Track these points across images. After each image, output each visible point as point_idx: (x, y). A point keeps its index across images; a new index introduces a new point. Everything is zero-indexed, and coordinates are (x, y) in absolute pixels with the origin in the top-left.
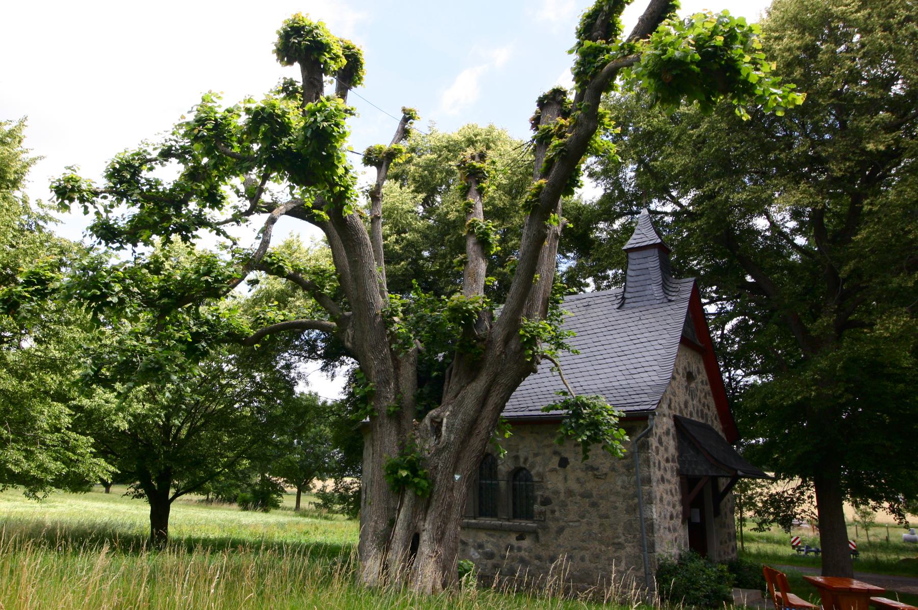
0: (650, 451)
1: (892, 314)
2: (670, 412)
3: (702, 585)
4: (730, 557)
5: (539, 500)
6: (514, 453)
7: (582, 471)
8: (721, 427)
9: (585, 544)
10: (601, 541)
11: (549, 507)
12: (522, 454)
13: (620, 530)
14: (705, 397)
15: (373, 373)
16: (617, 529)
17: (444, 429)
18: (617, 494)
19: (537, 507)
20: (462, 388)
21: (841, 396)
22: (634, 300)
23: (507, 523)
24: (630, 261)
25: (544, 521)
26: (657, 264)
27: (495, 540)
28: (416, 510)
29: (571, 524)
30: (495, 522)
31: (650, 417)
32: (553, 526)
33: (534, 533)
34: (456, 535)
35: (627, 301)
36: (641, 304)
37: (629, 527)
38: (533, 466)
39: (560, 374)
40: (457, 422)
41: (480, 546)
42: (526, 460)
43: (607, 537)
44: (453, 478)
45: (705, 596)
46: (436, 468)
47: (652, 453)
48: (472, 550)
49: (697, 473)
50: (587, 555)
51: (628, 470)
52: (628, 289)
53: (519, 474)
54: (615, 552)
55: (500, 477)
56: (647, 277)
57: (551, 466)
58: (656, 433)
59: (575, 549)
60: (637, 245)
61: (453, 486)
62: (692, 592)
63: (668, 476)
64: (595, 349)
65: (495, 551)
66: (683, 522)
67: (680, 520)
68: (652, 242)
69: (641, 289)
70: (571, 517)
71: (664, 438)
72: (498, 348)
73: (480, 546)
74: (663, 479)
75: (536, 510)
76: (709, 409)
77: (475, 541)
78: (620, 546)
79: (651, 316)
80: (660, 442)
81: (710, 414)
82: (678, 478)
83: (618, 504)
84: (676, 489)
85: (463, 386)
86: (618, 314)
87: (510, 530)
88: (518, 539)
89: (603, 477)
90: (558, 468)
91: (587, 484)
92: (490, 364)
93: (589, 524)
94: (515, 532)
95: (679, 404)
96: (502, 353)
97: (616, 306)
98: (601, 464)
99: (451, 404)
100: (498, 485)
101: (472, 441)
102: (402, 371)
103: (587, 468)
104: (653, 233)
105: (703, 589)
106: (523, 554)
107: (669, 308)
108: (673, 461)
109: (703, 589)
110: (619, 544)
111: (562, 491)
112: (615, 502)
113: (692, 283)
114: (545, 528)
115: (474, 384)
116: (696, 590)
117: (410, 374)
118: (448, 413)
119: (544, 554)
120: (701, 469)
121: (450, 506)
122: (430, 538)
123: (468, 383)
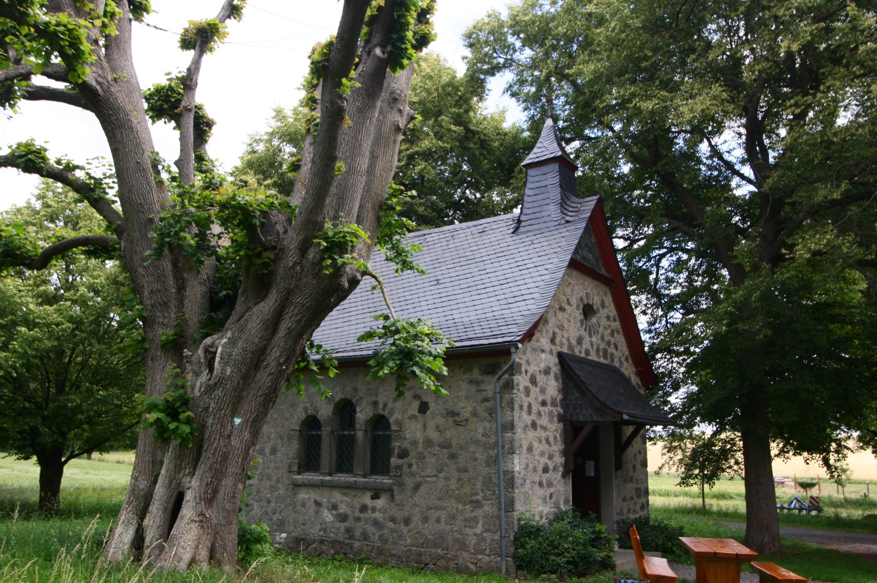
0: (515, 391)
1: (817, 232)
2: (553, 348)
3: (566, 549)
4: (637, 516)
5: (396, 452)
6: (374, 399)
7: (442, 417)
8: (634, 369)
9: (440, 503)
10: (458, 499)
11: (406, 460)
12: (381, 400)
13: (479, 486)
14: (612, 334)
15: (146, 293)
16: (475, 485)
17: (217, 359)
18: (478, 442)
19: (394, 461)
20: (249, 309)
21: (759, 331)
22: (530, 222)
23: (362, 479)
24: (529, 178)
25: (400, 476)
26: (557, 180)
27: (349, 500)
28: (181, 462)
29: (428, 479)
30: (352, 479)
31: (513, 350)
32: (409, 482)
33: (389, 490)
34: (234, 493)
35: (523, 224)
36: (537, 227)
37: (488, 482)
38: (392, 413)
39: (383, 292)
40: (236, 351)
41: (334, 507)
42: (385, 405)
43: (465, 493)
44: (232, 422)
45: (568, 562)
46: (206, 409)
47: (519, 396)
48: (326, 511)
49: (581, 418)
50: (443, 516)
51: (490, 414)
52: (525, 211)
53: (379, 422)
54: (472, 511)
55: (357, 426)
56: (546, 196)
57: (410, 412)
58: (526, 372)
59: (431, 508)
60: (537, 160)
61: (231, 433)
62: (553, 557)
63: (544, 421)
64: (479, 278)
65: (349, 513)
66: (564, 476)
67: (560, 474)
68: (552, 156)
69: (538, 209)
70: (428, 471)
71: (540, 378)
72: (291, 257)
73: (334, 507)
74: (534, 425)
75: (392, 464)
76: (616, 348)
77: (329, 501)
78: (477, 504)
79: (544, 239)
80: (533, 381)
81: (617, 354)
82: (561, 425)
83: (478, 455)
84: (555, 438)
85: (250, 308)
86: (511, 239)
87: (364, 488)
88: (373, 498)
89: (464, 424)
90: (418, 414)
91: (447, 432)
92: (281, 279)
93: (447, 479)
94: (370, 490)
95: (568, 340)
96: (295, 264)
97: (512, 230)
98: (463, 408)
99: (231, 329)
100: (355, 435)
101: (259, 375)
102: (188, 292)
103: (447, 414)
104: (555, 145)
105: (566, 554)
106: (377, 515)
107: (565, 230)
108: (553, 404)
109: (566, 554)
110: (477, 502)
111: (421, 441)
112: (475, 453)
113: (594, 202)
114: (401, 485)
115: (262, 304)
116: (558, 555)
117: (198, 296)
118: (225, 340)
119: (399, 515)
120: (586, 415)
121: (225, 457)
122: (196, 498)
123: (256, 304)
